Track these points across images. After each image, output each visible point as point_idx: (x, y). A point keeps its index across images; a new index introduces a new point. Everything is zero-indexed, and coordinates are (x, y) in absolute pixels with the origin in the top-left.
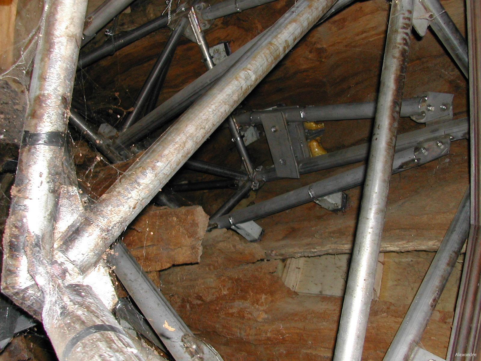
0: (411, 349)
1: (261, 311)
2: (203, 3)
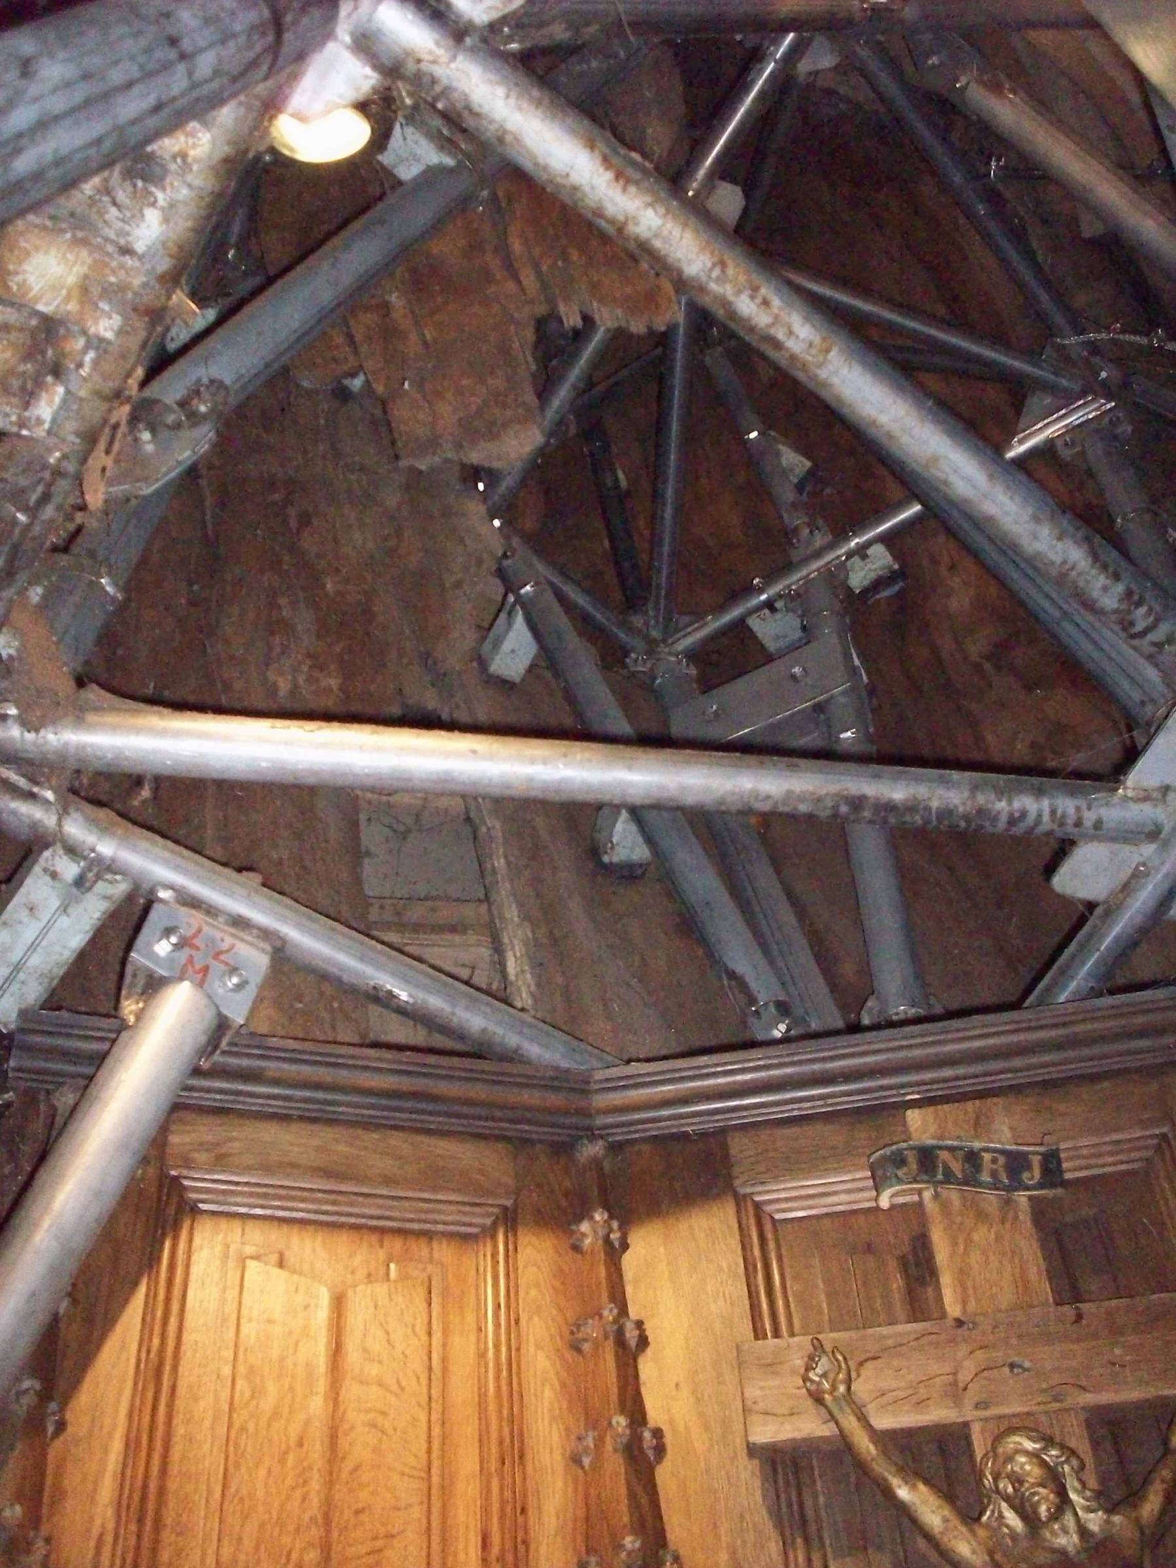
0: (266, 934)
1: (294, 678)
2: (1130, 429)
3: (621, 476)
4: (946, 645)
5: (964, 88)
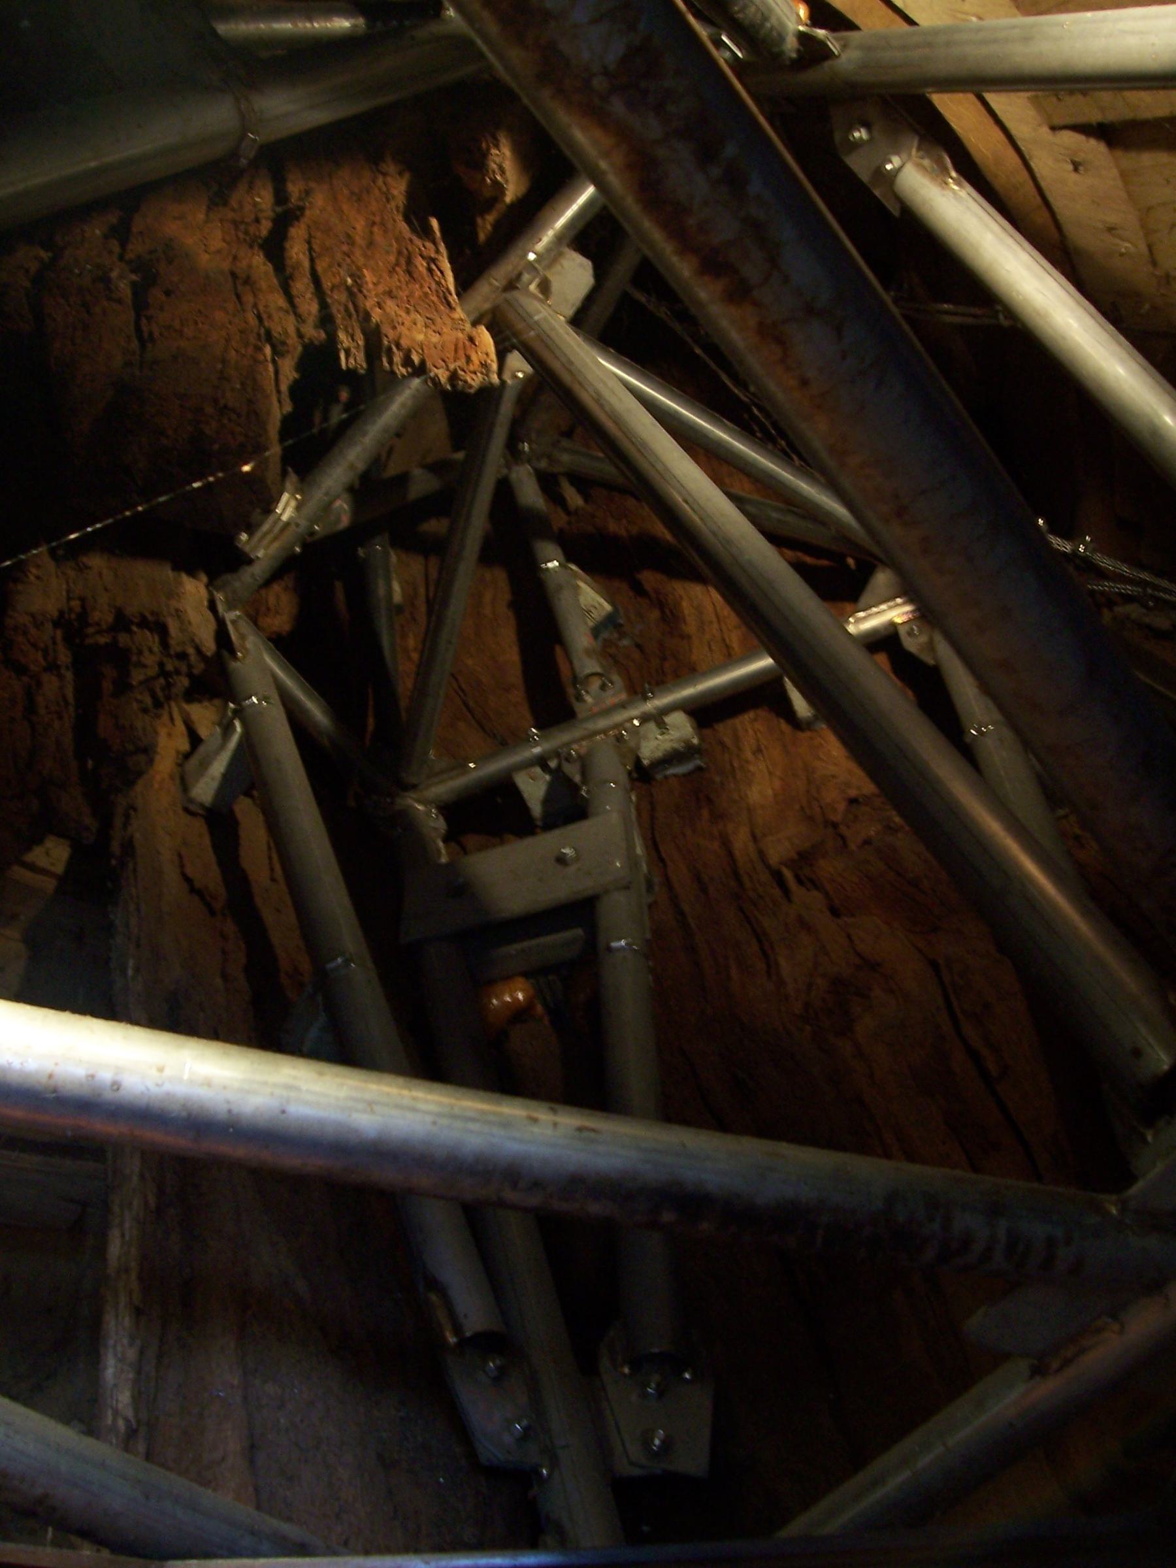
3: (396, 587)
4: (741, 840)
5: (898, 171)
